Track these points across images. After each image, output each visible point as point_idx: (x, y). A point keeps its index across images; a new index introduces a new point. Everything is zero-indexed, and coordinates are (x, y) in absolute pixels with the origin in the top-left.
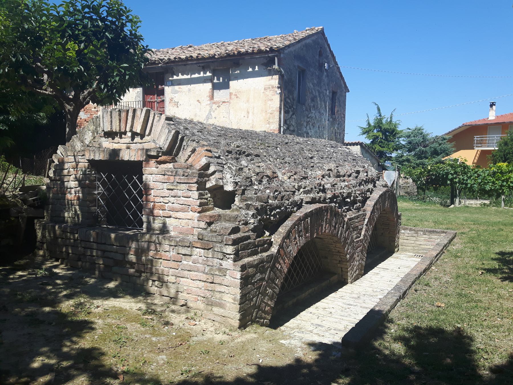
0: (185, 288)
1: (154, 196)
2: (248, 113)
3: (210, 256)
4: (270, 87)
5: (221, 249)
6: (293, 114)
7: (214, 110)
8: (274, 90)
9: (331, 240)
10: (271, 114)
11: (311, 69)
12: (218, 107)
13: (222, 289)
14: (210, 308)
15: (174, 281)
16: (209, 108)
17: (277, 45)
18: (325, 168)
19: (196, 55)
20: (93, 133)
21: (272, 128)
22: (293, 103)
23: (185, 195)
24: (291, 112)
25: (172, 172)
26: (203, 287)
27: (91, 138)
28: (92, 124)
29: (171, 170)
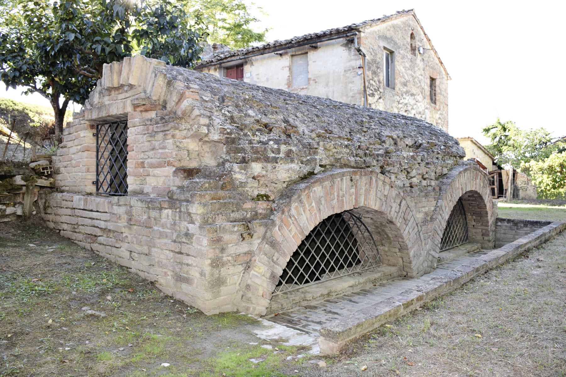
4: (351, 68)
6: (380, 98)
10: (352, 97)
11: (401, 52)
18: (383, 134)
22: (380, 86)
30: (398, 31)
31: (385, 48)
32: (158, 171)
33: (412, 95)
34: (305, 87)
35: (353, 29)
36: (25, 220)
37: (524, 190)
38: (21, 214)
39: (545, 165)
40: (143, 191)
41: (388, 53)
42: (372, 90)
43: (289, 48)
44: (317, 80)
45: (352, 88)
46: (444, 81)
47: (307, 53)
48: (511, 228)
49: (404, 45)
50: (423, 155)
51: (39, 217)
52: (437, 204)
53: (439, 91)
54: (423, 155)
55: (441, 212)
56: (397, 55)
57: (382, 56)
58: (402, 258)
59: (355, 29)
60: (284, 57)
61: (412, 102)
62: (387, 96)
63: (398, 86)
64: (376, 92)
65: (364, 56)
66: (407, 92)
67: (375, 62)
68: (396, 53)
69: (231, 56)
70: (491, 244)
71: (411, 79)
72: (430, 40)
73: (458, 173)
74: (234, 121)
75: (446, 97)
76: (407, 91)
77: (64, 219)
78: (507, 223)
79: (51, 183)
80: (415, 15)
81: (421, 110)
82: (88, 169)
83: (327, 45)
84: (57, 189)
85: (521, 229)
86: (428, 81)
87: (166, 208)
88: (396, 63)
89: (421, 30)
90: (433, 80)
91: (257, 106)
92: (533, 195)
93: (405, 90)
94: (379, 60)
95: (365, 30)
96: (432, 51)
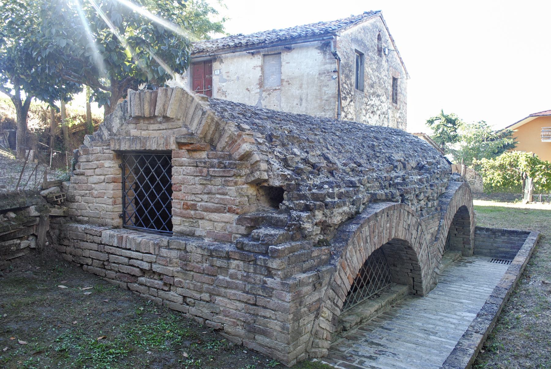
0: (222, 309)
1: (184, 193)
2: (301, 100)
3: (252, 270)
5: (265, 263)
6: (351, 101)
7: (264, 98)
8: (329, 75)
9: (402, 246)
10: (326, 100)
11: (370, 54)
12: (269, 94)
13: (268, 313)
14: (252, 335)
15: (208, 299)
17: (332, 27)
18: (393, 158)
19: (246, 41)
20: (121, 119)
21: (327, 116)
22: (351, 89)
23: (220, 191)
24: (348, 98)
25: (205, 163)
26: (243, 309)
27: (119, 125)
28: (120, 109)
29: (203, 160)
30: (367, 33)
31: (356, 51)
32: (215, 216)
33: (378, 96)
34: (277, 88)
35: (329, 32)
36: (39, 253)
37: (472, 184)
38: (34, 247)
39: (497, 163)
40: (194, 234)
41: (358, 55)
42: (344, 93)
43: (262, 48)
44: (290, 82)
45: (327, 92)
46: (405, 81)
47: (280, 53)
48: (489, 236)
49: (372, 47)
50: (427, 177)
51: (53, 248)
52: (440, 224)
53: (400, 90)
54: (427, 177)
55: (443, 231)
57: (353, 58)
58: (413, 278)
59: (332, 33)
60: (256, 56)
61: (378, 103)
62: (357, 99)
63: (367, 88)
64: (348, 95)
65: (339, 60)
66: (374, 94)
67: (348, 65)
68: (366, 56)
69: (199, 52)
70: (471, 252)
71: (377, 81)
72: (393, 41)
73: (454, 192)
74: (287, 163)
75: (405, 96)
76: (373, 92)
77: (87, 253)
78: (486, 232)
79: (64, 212)
80: (382, 16)
81: (384, 110)
82: (115, 202)
83: (301, 47)
84: (71, 218)
85: (499, 238)
86: (391, 81)
87: (235, 259)
88: (365, 65)
89: (386, 31)
90: (395, 79)
91: (297, 142)
92: (480, 188)
93: (372, 91)
94: (351, 63)
95: (340, 34)
96: (395, 52)
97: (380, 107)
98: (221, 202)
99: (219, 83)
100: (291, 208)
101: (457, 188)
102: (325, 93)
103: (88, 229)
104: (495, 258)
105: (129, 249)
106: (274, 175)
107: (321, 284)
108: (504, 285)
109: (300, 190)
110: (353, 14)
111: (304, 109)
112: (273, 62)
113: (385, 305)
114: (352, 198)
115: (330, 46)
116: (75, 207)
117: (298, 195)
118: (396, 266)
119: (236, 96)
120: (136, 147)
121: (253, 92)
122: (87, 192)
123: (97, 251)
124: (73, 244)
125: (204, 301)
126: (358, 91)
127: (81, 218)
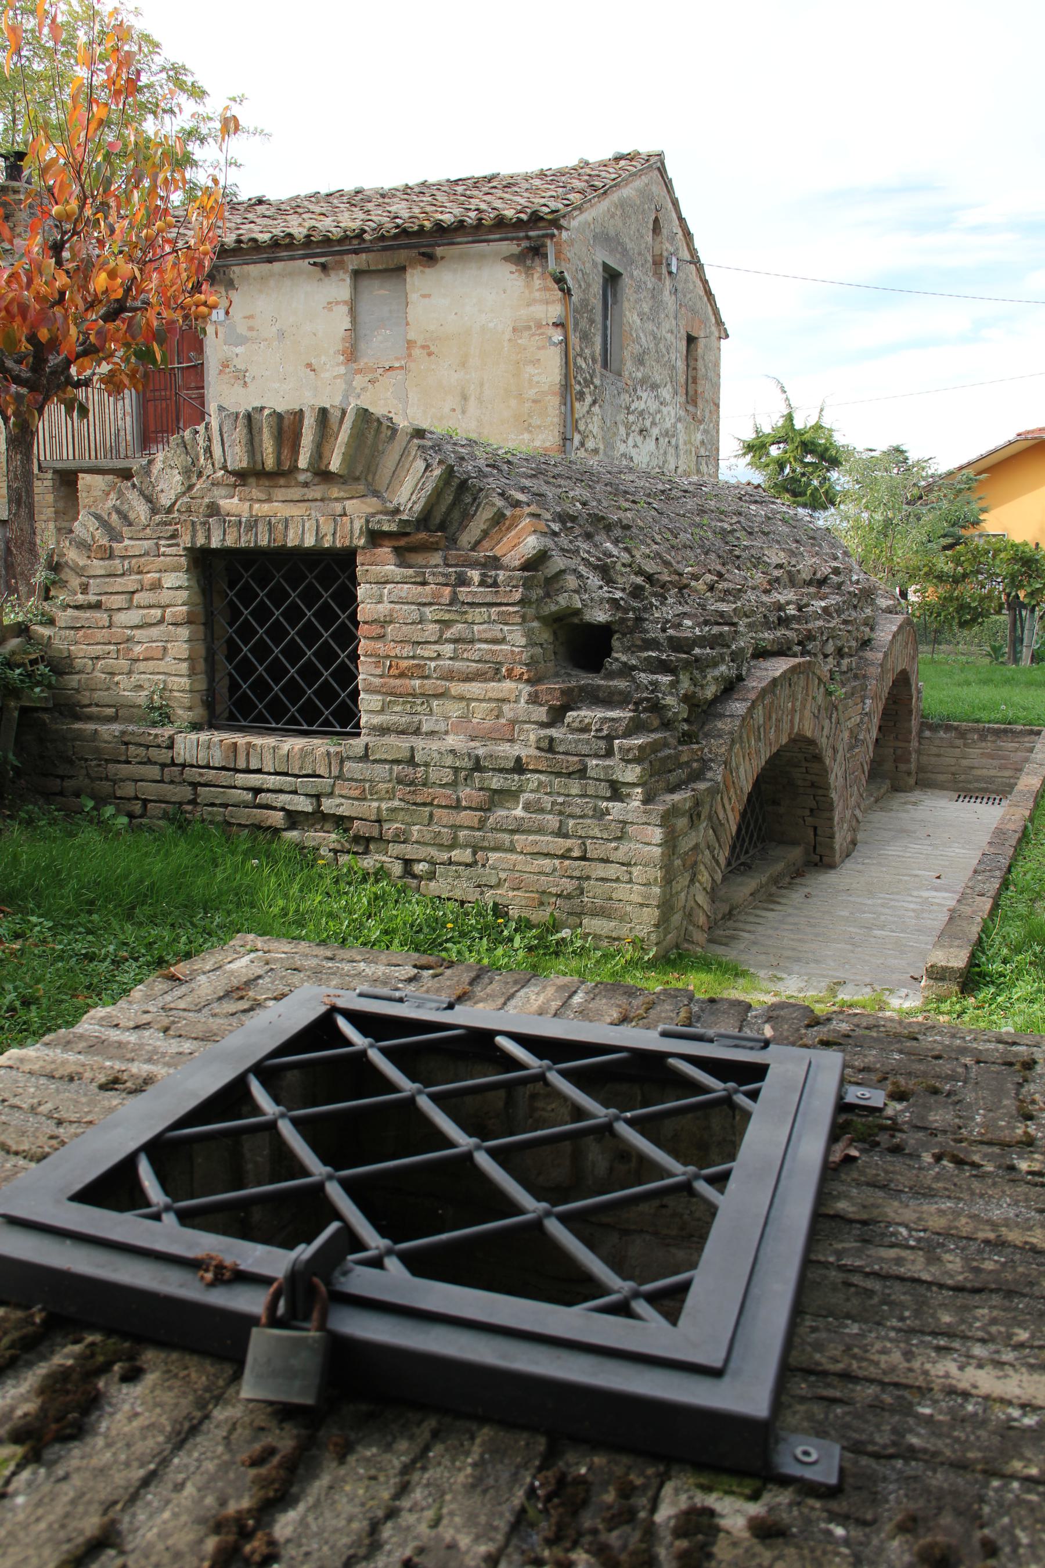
4: (532, 324)
5: (606, 774)
6: (594, 402)
7: (358, 390)
10: (535, 401)
13: (612, 871)
16: (344, 386)
19: (305, 232)
21: (537, 444)
22: (594, 370)
33: (655, 387)
35: (542, 219)
42: (579, 383)
44: (432, 348)
49: (640, 254)
56: (627, 283)
58: (815, 829)
60: (332, 273)
61: (653, 406)
63: (629, 366)
64: (588, 386)
66: (643, 381)
67: (587, 305)
68: (626, 280)
70: (912, 781)
71: (652, 346)
75: (716, 386)
81: (668, 425)
83: (463, 258)
86: (683, 345)
90: (691, 340)
93: (639, 375)
97: (659, 416)
98: (487, 658)
99: (225, 348)
100: (634, 668)
101: (895, 628)
102: (530, 381)
103: (133, 733)
104: (963, 794)
105: (259, 771)
106: (592, 599)
107: (699, 815)
108: (1012, 826)
109: (646, 631)
110: (586, 158)
111: (473, 425)
112: (382, 292)
113: (767, 884)
114: (729, 647)
115: (545, 256)
116: (75, 685)
117: (644, 640)
118: (779, 804)
119: (277, 385)
120: (256, 542)
121: (326, 375)
122: (112, 647)
123: (162, 781)
124: (84, 772)
125: (460, 864)
126: (608, 374)
127: (94, 709)
